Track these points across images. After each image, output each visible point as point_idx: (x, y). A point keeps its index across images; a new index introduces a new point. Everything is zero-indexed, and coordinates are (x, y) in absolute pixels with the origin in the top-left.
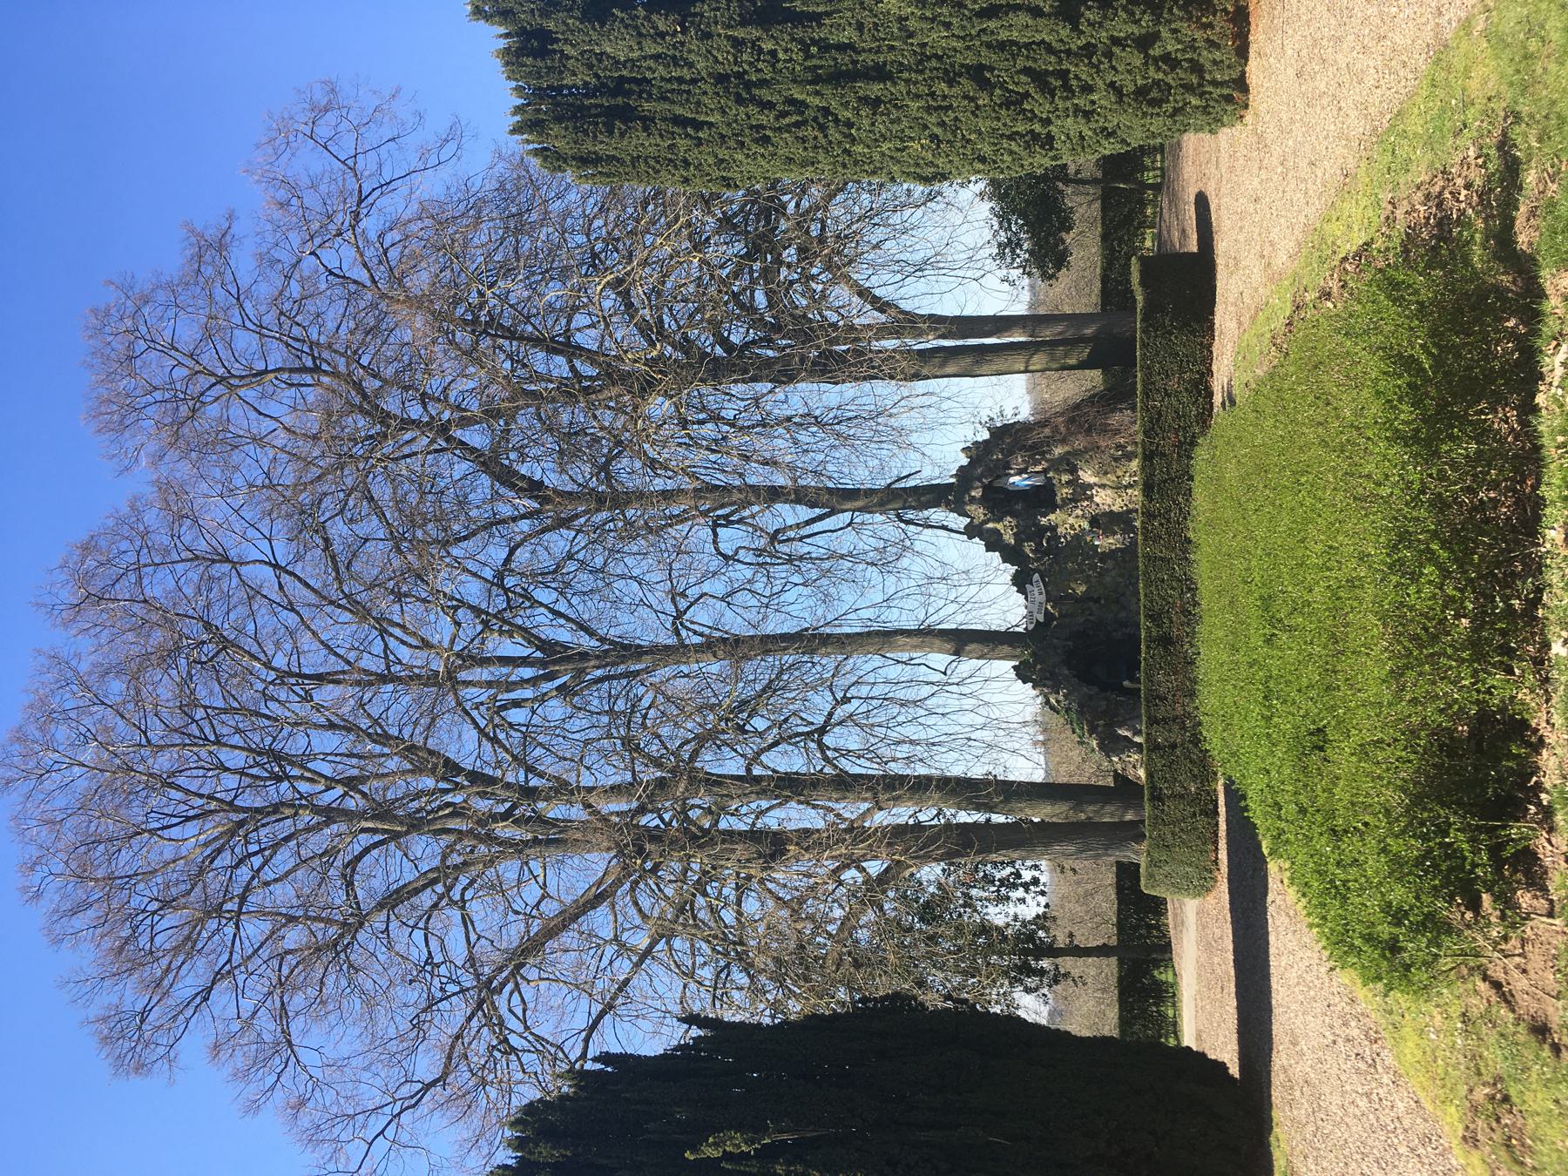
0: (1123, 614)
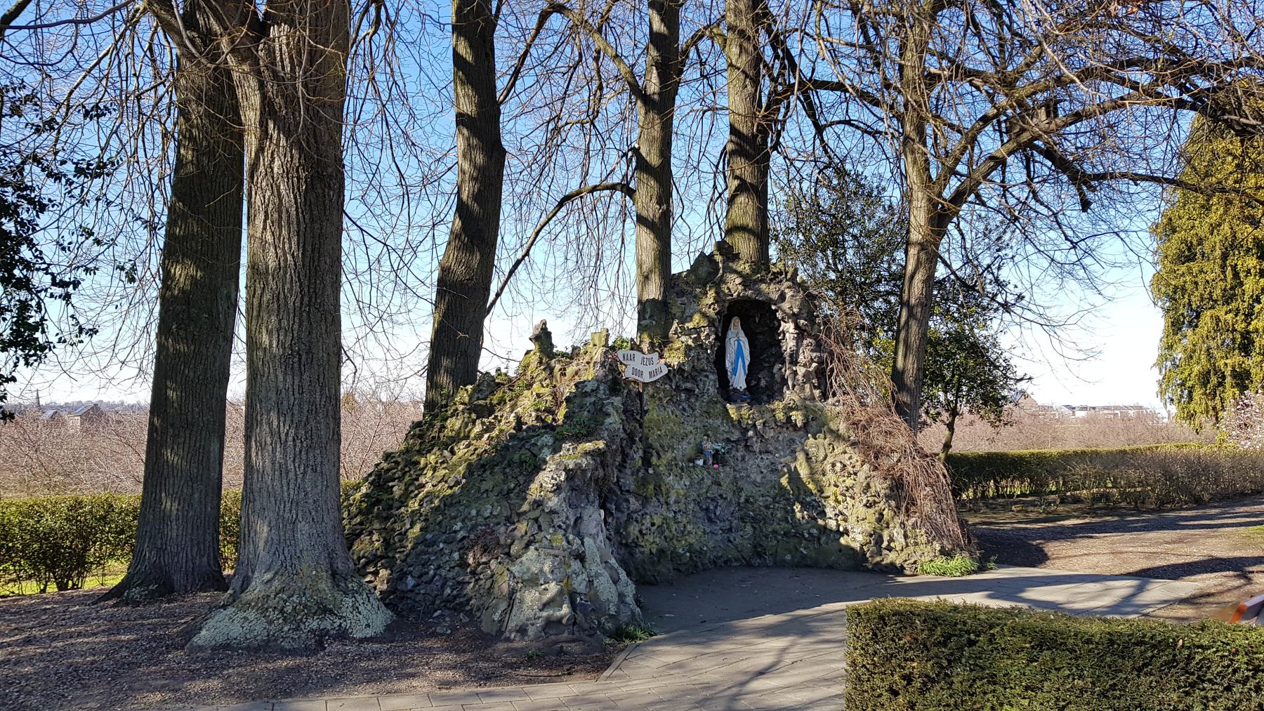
0: (634, 504)
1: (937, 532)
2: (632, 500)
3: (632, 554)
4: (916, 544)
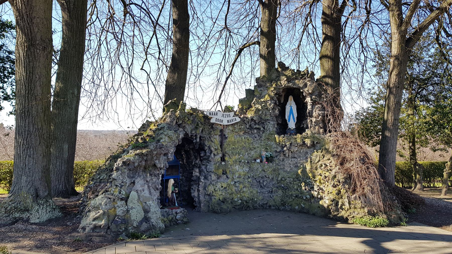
0: (214, 177)
1: (367, 202)
2: (213, 175)
3: (211, 199)
4: (355, 208)
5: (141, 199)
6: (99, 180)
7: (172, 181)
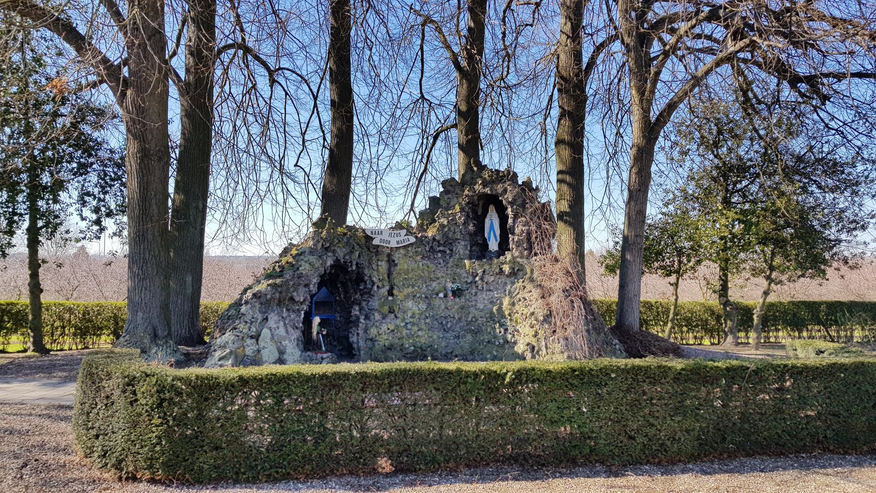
0: (377, 316)
2: (376, 314)
3: (374, 345)
4: (553, 353)
5: (276, 338)
6: (226, 317)
7: (317, 320)
